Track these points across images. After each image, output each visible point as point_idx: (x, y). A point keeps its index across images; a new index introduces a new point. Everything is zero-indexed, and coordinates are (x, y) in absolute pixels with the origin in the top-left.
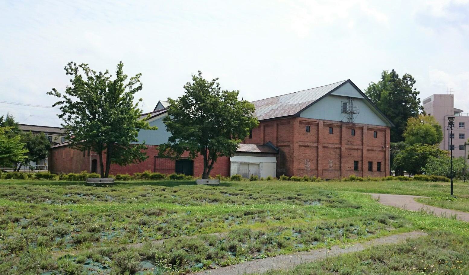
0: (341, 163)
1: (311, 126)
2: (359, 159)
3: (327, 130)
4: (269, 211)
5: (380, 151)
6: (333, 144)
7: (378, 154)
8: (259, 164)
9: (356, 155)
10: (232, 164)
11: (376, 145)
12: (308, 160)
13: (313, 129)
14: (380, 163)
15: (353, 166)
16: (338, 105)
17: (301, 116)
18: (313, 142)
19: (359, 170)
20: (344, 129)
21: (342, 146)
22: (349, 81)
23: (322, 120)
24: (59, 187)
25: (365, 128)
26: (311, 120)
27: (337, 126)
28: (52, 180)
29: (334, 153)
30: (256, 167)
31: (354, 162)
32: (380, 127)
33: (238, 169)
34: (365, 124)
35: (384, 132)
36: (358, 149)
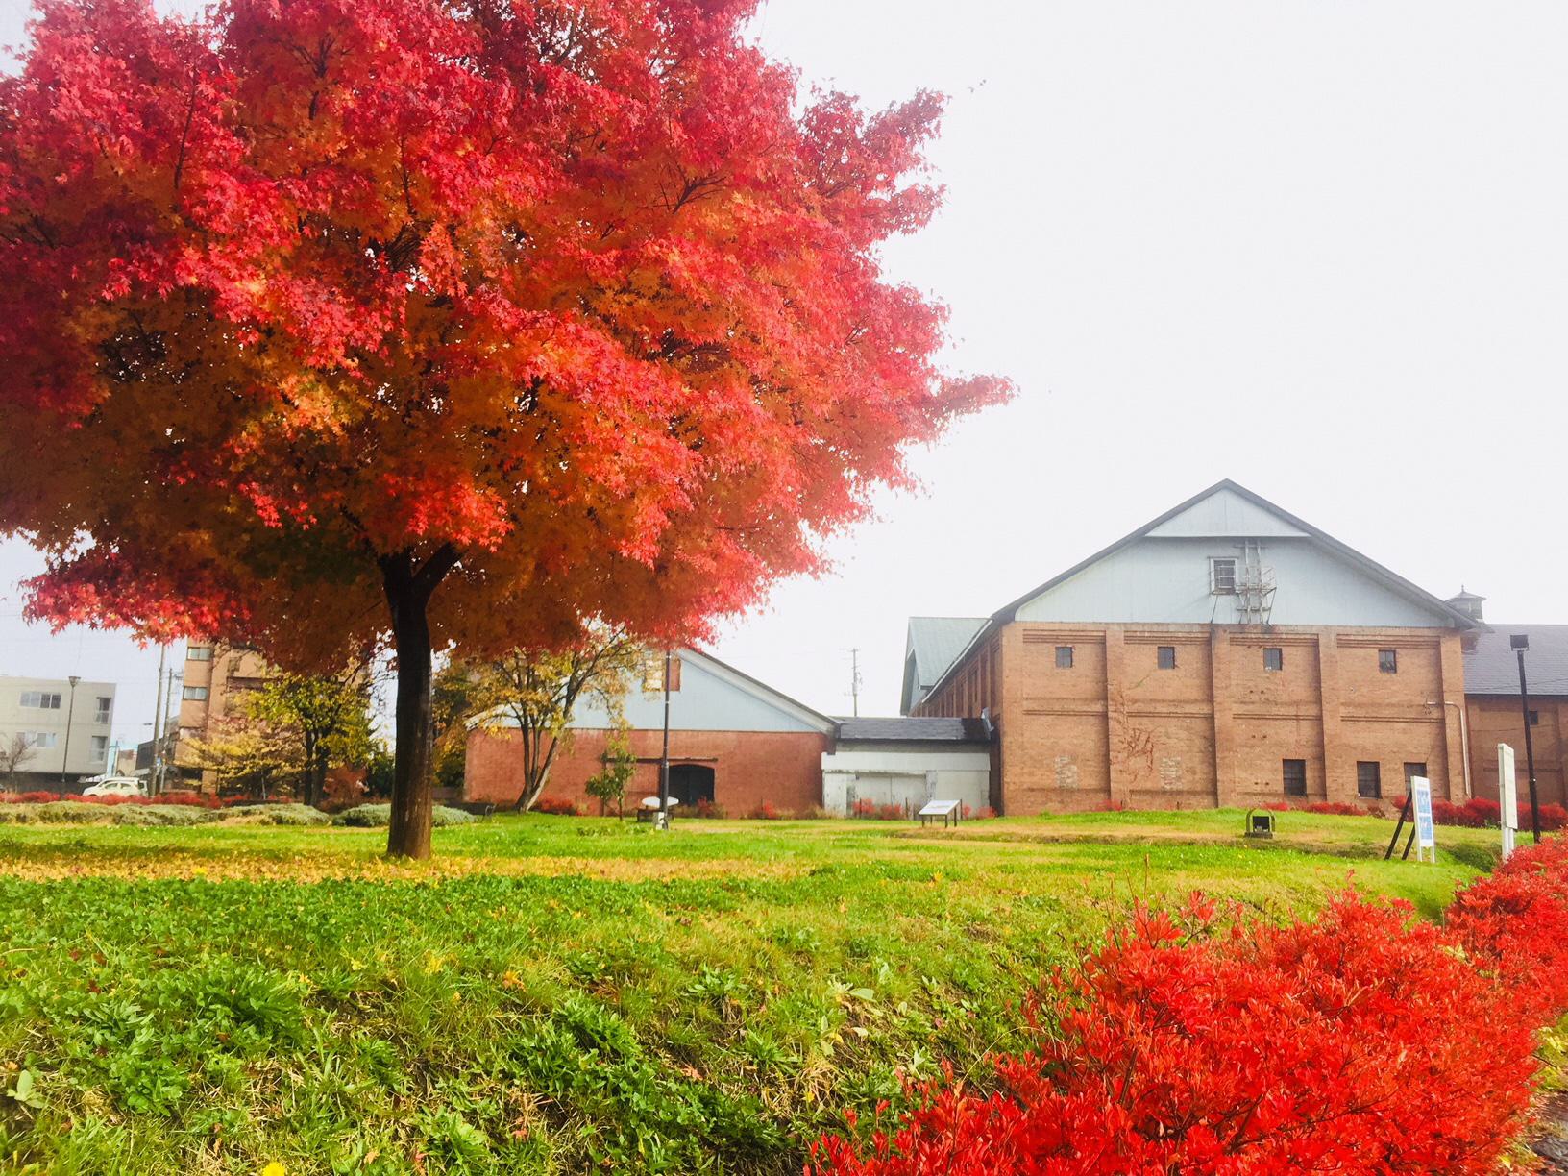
0: (1213, 765)
1: (1077, 646)
2: (1305, 754)
3: (1149, 655)
4: (293, 918)
5: (1416, 720)
6: (1297, 704)
7: (1404, 731)
8: (925, 777)
9: (1294, 739)
10: (861, 714)
11: (1394, 700)
12: (1066, 759)
13: (1085, 655)
14: (1301, 763)
15: (1280, 777)
16: (1198, 571)
17: (1018, 616)
18: (1086, 699)
19: (1308, 791)
20: (1222, 647)
21: (1217, 708)
22: (1228, 487)
23: (1119, 624)
24: (792, 827)
25: (1114, 640)
26: (1071, 627)
27: (1188, 641)
28: (710, 815)
29: (1183, 734)
30: (919, 783)
31: (1280, 765)
32: (1407, 632)
33: (850, 792)
34: (1326, 627)
35: (1432, 652)
36: (1297, 718)
